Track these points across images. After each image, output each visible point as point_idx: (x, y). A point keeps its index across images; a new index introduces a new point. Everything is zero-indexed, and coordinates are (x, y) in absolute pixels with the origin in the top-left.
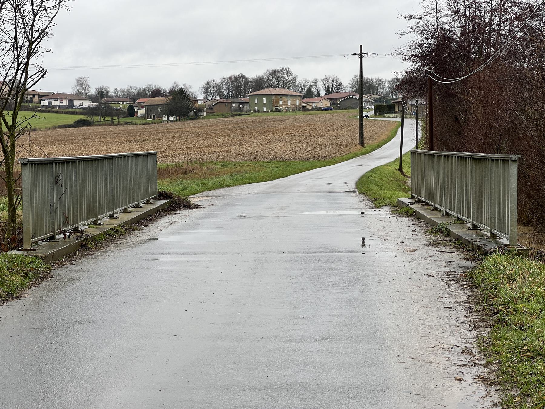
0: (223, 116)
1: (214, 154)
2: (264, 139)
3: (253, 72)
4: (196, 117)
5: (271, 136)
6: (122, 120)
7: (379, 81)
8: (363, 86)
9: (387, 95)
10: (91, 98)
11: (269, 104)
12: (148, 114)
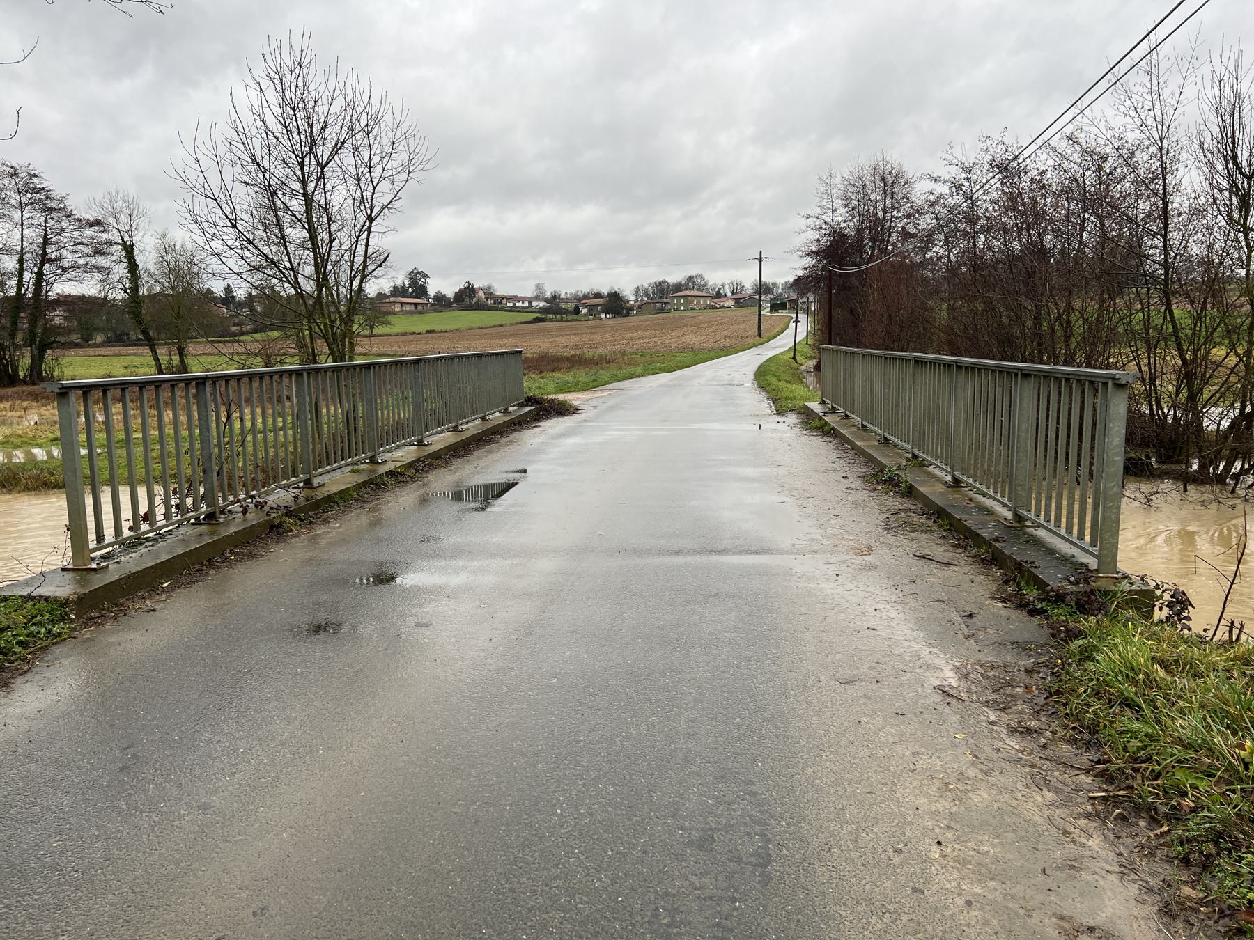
0: (650, 314)
1: (637, 345)
2: (679, 333)
3: (673, 279)
4: (628, 315)
5: (685, 329)
6: (570, 318)
7: (774, 284)
8: (762, 288)
9: (781, 295)
10: (546, 300)
11: (686, 304)
12: (590, 313)
